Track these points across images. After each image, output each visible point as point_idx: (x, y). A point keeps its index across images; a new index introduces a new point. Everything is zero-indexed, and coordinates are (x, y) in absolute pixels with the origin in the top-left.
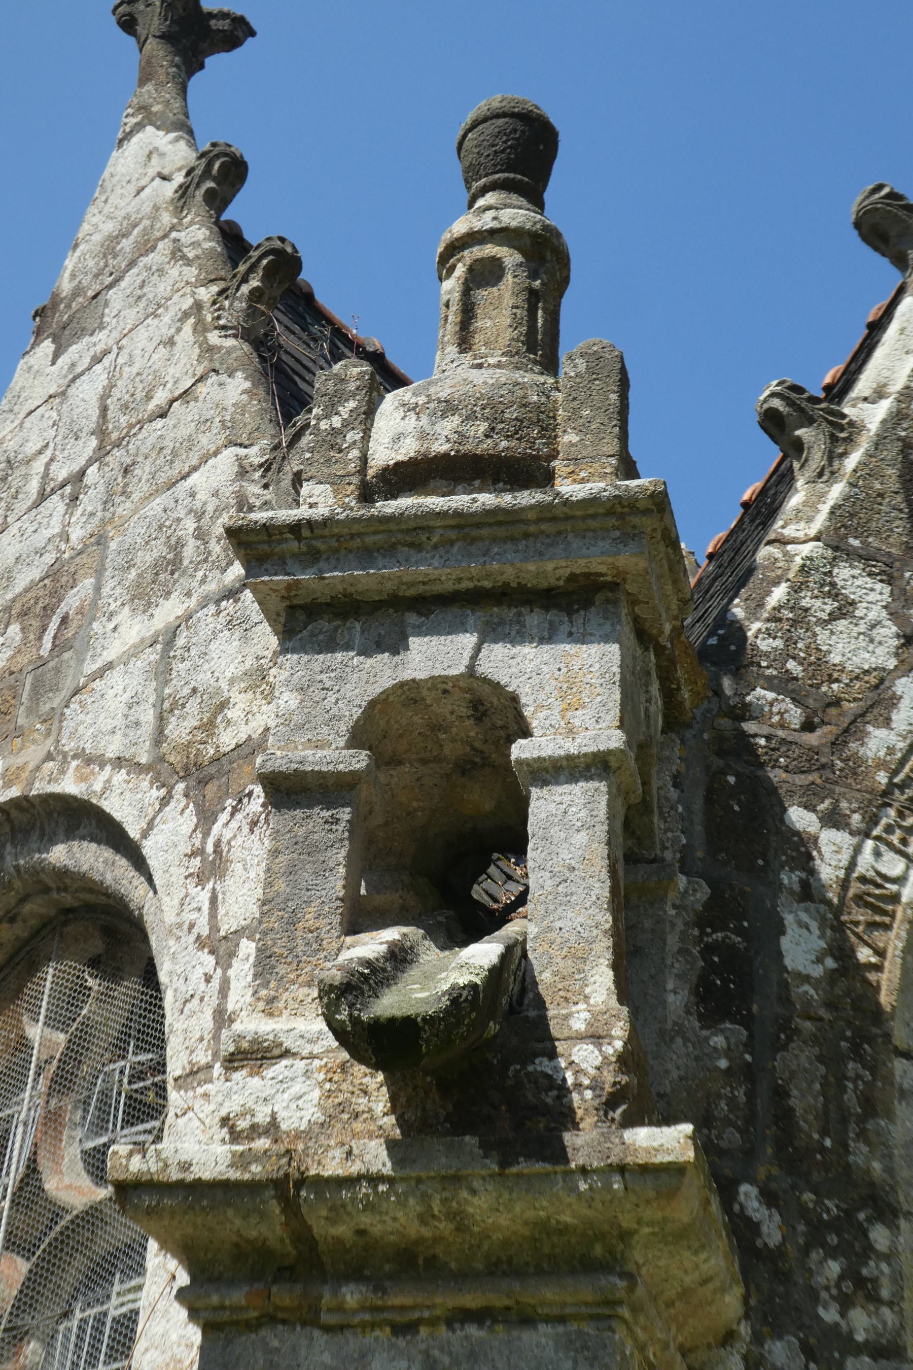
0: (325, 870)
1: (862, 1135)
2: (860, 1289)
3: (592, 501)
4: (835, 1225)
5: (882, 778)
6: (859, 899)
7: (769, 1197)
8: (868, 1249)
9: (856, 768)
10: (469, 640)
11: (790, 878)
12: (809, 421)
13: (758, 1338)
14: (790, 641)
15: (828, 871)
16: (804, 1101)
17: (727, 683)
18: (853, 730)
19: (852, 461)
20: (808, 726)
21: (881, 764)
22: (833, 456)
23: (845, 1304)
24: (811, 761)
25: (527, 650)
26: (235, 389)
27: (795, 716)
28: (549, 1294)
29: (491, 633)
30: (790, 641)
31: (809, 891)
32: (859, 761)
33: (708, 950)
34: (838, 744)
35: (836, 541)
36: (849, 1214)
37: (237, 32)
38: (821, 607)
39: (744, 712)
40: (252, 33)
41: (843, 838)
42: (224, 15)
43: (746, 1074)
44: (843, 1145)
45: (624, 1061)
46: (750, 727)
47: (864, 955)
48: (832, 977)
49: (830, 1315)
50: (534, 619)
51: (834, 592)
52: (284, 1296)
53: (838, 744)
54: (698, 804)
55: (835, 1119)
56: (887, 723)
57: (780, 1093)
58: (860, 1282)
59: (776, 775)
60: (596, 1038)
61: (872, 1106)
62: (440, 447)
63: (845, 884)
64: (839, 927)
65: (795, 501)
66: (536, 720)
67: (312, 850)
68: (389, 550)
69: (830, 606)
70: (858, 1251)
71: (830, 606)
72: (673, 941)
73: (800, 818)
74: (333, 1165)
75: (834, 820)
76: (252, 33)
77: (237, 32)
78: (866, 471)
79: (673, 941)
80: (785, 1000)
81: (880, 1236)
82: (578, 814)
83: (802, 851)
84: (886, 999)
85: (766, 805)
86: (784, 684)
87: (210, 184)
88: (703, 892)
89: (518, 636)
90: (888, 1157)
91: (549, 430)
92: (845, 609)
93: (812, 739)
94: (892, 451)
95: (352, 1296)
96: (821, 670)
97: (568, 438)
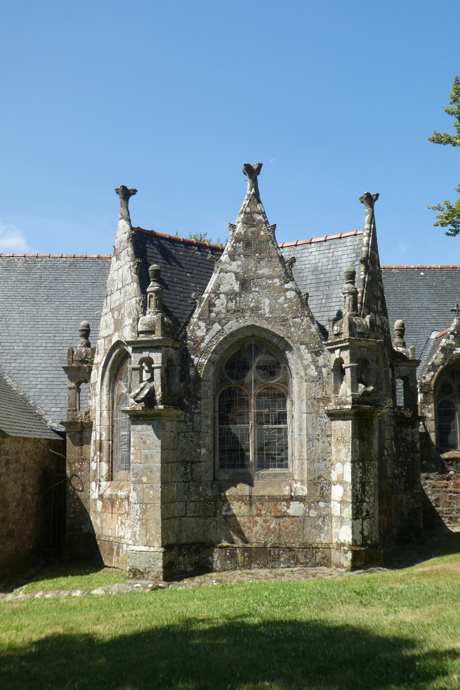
0: (137, 377)
1: (198, 392)
2: (196, 408)
3: (157, 339)
4: (194, 402)
5: (203, 350)
6: (199, 365)
7: (187, 400)
8: (198, 403)
9: (200, 349)
10: (148, 352)
11: (191, 364)
12: (197, 299)
13: (185, 414)
14: (192, 334)
15: (195, 363)
16: (191, 389)
17: (184, 341)
18: (200, 344)
19: (202, 304)
20: (194, 345)
21: (203, 348)
22: (200, 304)
23: (195, 409)
24: (194, 349)
25: (153, 353)
26: (135, 286)
27: (193, 343)
28: (155, 418)
29: (150, 352)
30: (192, 334)
31: (193, 365)
32: (200, 348)
33: (181, 375)
34: (197, 346)
35: (199, 319)
36: (196, 400)
37: (135, 191)
38: (196, 328)
39: (187, 344)
40: (137, 191)
41: (197, 358)
42: (132, 190)
43: (185, 388)
44: (195, 393)
45: (161, 398)
46: (187, 346)
47: (199, 372)
48: (195, 375)
49: (193, 411)
50: (154, 350)
51: (198, 326)
52: (136, 418)
53: (197, 346)
54: (180, 358)
55: (195, 391)
56: (204, 342)
57: (189, 389)
58: (196, 407)
59: (190, 352)
60: (159, 395)
61: (199, 388)
62: (144, 330)
63: (197, 364)
64: (196, 369)
65: (196, 310)
66: (155, 362)
67: (136, 375)
68: (139, 343)
69: (198, 328)
70: (196, 404)
71: (198, 328)
72: (177, 374)
73: (192, 357)
74: (137, 409)
75: (196, 356)
76: (137, 191)
77: (135, 191)
78: (204, 306)
79: (177, 374)
80: (190, 379)
81: (199, 402)
82: (158, 372)
83: (192, 360)
84: (201, 377)
85: (189, 355)
86: (191, 340)
87: (131, 239)
88: (181, 368)
89: (153, 352)
90: (200, 394)
91: (155, 327)
92: (199, 328)
93: (195, 346)
94: (207, 303)
95: (141, 418)
96: (196, 337)
97: (156, 328)
